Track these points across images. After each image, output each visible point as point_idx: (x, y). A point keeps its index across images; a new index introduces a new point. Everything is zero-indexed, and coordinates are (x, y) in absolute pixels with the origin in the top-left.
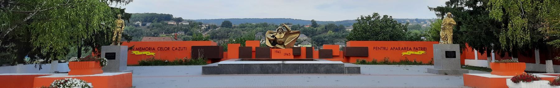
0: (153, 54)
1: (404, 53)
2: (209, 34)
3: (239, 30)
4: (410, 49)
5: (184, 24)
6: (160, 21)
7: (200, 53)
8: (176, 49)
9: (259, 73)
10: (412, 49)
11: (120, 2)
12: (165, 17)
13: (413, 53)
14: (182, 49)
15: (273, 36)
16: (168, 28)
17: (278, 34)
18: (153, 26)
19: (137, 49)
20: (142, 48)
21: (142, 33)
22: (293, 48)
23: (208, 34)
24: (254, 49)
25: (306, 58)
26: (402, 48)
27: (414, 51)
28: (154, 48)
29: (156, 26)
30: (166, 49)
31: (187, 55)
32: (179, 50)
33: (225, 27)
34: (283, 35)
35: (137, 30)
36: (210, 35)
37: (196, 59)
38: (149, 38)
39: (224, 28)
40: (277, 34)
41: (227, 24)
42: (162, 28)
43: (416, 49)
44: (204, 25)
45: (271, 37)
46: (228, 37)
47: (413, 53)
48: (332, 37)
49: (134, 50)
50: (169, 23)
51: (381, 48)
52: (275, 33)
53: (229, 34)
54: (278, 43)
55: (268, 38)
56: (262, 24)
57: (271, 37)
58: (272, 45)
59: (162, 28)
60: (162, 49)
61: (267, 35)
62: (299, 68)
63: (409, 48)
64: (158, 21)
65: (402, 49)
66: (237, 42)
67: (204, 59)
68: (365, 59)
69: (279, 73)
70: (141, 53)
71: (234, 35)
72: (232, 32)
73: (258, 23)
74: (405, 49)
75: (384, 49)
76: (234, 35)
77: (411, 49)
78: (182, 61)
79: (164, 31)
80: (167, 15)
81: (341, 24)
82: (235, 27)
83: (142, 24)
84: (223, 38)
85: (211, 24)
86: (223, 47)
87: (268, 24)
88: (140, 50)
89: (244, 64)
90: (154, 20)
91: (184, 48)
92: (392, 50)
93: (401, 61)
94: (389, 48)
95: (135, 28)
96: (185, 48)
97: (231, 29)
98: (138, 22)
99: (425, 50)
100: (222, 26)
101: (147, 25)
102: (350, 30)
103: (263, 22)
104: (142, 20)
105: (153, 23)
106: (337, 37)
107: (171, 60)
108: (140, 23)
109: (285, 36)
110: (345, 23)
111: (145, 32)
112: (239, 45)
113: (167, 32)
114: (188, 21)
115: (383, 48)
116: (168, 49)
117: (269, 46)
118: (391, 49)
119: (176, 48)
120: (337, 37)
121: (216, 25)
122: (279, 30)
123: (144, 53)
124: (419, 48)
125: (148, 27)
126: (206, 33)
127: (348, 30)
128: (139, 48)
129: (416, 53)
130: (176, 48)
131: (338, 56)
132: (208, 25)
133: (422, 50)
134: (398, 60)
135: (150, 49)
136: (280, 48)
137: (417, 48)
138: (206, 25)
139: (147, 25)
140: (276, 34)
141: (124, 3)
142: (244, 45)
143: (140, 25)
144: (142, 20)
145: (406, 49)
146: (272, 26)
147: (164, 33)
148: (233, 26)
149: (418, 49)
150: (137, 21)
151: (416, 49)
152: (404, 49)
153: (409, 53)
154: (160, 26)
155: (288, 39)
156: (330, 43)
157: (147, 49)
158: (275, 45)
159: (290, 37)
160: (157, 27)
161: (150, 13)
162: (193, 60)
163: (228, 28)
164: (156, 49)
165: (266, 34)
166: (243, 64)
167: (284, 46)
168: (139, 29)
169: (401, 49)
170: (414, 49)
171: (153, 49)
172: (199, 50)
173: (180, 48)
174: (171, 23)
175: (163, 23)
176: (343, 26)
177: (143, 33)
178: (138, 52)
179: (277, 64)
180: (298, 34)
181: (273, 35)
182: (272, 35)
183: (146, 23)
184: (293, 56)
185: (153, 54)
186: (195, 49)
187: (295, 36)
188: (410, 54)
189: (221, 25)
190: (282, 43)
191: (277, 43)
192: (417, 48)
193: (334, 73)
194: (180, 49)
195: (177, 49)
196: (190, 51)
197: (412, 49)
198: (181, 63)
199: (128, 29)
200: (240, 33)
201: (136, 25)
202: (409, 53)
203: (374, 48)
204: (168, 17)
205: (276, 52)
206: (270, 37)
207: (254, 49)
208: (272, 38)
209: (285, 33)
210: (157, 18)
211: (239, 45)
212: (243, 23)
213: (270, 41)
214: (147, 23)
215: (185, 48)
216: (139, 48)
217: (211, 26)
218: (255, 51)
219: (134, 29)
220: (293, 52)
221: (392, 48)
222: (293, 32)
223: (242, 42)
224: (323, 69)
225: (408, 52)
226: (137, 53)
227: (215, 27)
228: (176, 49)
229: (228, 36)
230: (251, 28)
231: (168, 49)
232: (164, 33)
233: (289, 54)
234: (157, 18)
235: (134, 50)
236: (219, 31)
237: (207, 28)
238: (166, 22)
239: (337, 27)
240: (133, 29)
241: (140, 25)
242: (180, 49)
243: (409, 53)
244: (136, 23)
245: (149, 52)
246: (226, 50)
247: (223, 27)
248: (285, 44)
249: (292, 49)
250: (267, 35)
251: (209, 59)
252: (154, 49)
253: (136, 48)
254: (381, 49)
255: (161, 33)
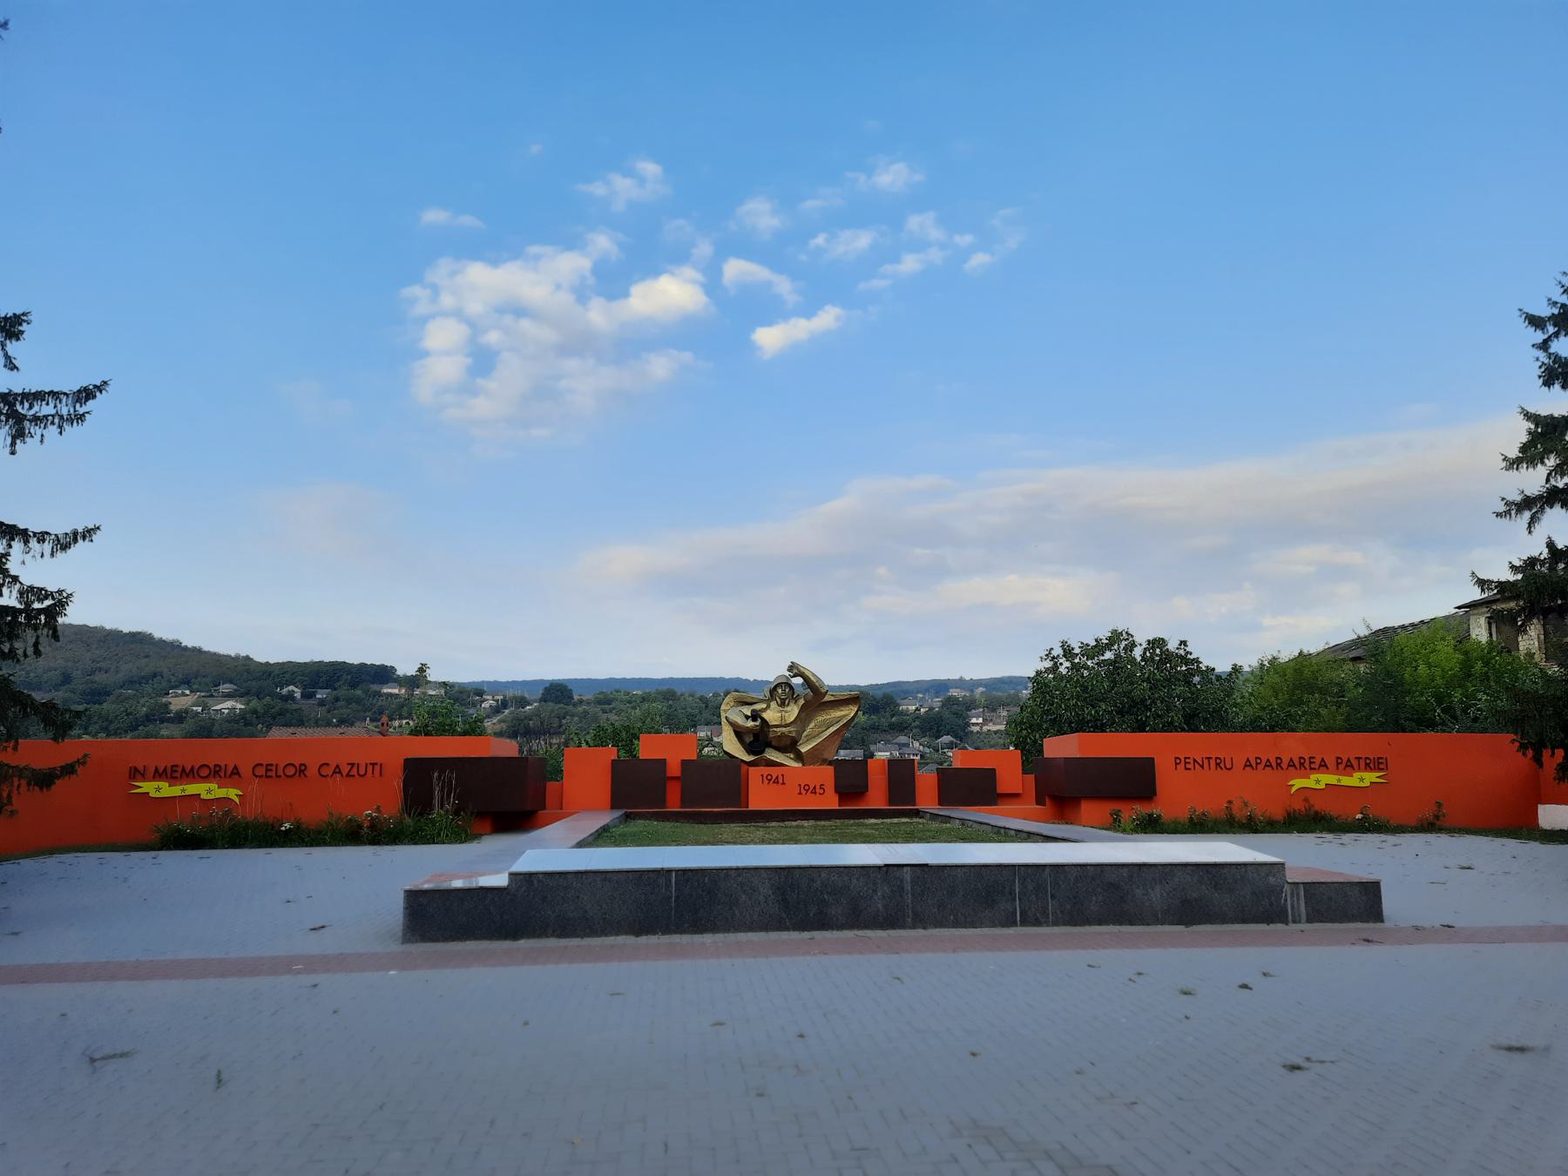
0: (233, 793)
1: (1298, 783)
2: (504, 721)
3: (593, 709)
4: (1323, 767)
5: (431, 692)
6: (358, 685)
7: (442, 790)
8: (337, 770)
9: (765, 927)
10: (1331, 762)
11: (26, 542)
12: (373, 671)
13: (1331, 779)
14: (362, 773)
15: (755, 716)
16: (381, 706)
17: (773, 704)
18: (337, 699)
19: (159, 775)
20: (183, 770)
21: (302, 721)
22: (838, 764)
23: (500, 721)
24: (674, 769)
25: (891, 801)
26: (1291, 760)
27: (1337, 772)
28: (235, 767)
29: (344, 699)
30: (291, 771)
31: (385, 800)
32: (348, 775)
33: (552, 701)
34: (793, 712)
35: (287, 711)
36: (506, 724)
37: (421, 814)
38: (291, 730)
39: (550, 704)
40: (768, 707)
41: (559, 693)
42: (364, 706)
43: (1348, 767)
44: (489, 697)
45: (747, 717)
46: (561, 730)
47: (1331, 779)
48: (863, 729)
49: (143, 775)
50: (385, 691)
51: (1206, 761)
52: (762, 701)
53: (564, 721)
54: (773, 743)
55: (733, 724)
56: (658, 693)
57: (747, 717)
58: (750, 751)
59: (364, 706)
60: (273, 774)
61: (725, 711)
62: (1012, 892)
63: (1318, 761)
64: (353, 686)
65: (1291, 764)
66: (600, 741)
67: (456, 813)
68: (1140, 809)
69: (891, 920)
70: (176, 791)
71: (580, 725)
72: (573, 716)
73: (647, 691)
74: (1301, 764)
75: (1367, 764)
76: (580, 725)
77: (1326, 766)
78: (360, 827)
79: (368, 714)
80: (378, 666)
81: (888, 691)
82: (581, 702)
83: (302, 694)
84: (544, 734)
85: (510, 693)
86: (542, 761)
87: (679, 694)
88: (172, 777)
89: (677, 871)
90: (338, 681)
91: (370, 767)
92: (1268, 769)
93: (1289, 814)
94: (1239, 763)
95: (279, 705)
96: (377, 768)
97: (570, 707)
98: (291, 688)
99: (1380, 770)
100: (544, 700)
101: (318, 696)
102: (910, 707)
103: (664, 688)
104: (302, 682)
105: (335, 689)
106: (874, 728)
107: (313, 814)
108: (296, 690)
109: (803, 715)
110: (893, 689)
111: (312, 716)
112: (611, 752)
113: (377, 716)
114: (445, 684)
115: (1213, 762)
116: (301, 771)
117: (737, 755)
118: (1246, 766)
119: (337, 766)
120: (874, 728)
121: (526, 695)
122: (780, 691)
123: (192, 789)
124: (1359, 758)
125: (322, 703)
126: (495, 721)
127: (904, 707)
128: (169, 770)
129: (1346, 781)
130: (337, 766)
131: (1016, 795)
132: (502, 697)
133: (1368, 767)
134: (1278, 814)
135: (216, 772)
136: (782, 765)
137: (1349, 760)
138: (496, 697)
139: (318, 696)
140: (764, 706)
141: (47, 547)
142: (631, 751)
143: (298, 695)
144: (302, 682)
145: (1305, 766)
146: (691, 698)
147: (368, 719)
148: (576, 697)
149: (1354, 762)
150: (288, 685)
151: (1346, 766)
152: (1274, 765)
153: (1362, 780)
154: (358, 701)
155: (812, 725)
156: (855, 746)
157: (205, 772)
158: (763, 752)
159: (820, 718)
160: (349, 701)
161: (327, 660)
162: (408, 821)
163: (562, 705)
164: (246, 770)
165: (723, 707)
166: (669, 871)
167: (799, 757)
168: (295, 707)
169: (1284, 765)
170: (1338, 764)
171: (232, 773)
172: (436, 775)
173: (356, 767)
174: (389, 691)
175: (366, 692)
176: (892, 698)
177: (305, 719)
178: (164, 785)
179: (879, 867)
180: (851, 707)
181: (753, 711)
182: (747, 711)
183: (316, 692)
184: (836, 798)
185: (233, 793)
186: (418, 773)
187: (843, 713)
188: (1322, 786)
189: (540, 696)
190: (788, 743)
191: (769, 745)
192: (1349, 760)
193: (1224, 920)
194: (354, 772)
195: (340, 772)
196: (395, 782)
197: (1331, 762)
198: (352, 834)
199: (259, 709)
200: (596, 719)
201: (283, 695)
202: (1319, 780)
203: (1176, 764)
204: (384, 674)
205: (766, 781)
206: (740, 720)
207: (674, 769)
208: (750, 724)
209: (802, 702)
210: (349, 677)
211: (611, 752)
212: (604, 691)
213: (739, 733)
214: (319, 690)
215: (377, 768)
216: (169, 770)
217: (510, 699)
218: (678, 778)
219: (277, 708)
220: (836, 777)
221: (1248, 760)
222: (832, 699)
223: (625, 738)
224: (1156, 896)
225: (1314, 777)
226: (158, 789)
227: (522, 702)
228: (337, 770)
229: (560, 726)
230: (628, 705)
231: (302, 770)
232: (368, 719)
233: (818, 790)
234: (349, 677)
235: (143, 775)
236: (537, 713)
237: (497, 707)
238: (375, 687)
239: (875, 699)
240: (273, 708)
241: (298, 695)
242: (353, 772)
243: (1319, 780)
244: (285, 691)
245: (214, 786)
246: (558, 772)
247: (545, 701)
248: (804, 749)
249: (831, 768)
250: (725, 711)
251: (481, 815)
252: (236, 772)
253: (156, 770)
254: (1206, 765)
255: (359, 720)
